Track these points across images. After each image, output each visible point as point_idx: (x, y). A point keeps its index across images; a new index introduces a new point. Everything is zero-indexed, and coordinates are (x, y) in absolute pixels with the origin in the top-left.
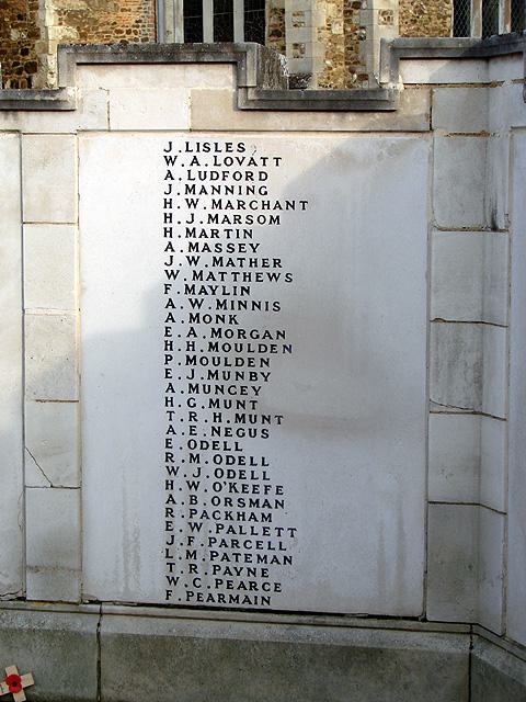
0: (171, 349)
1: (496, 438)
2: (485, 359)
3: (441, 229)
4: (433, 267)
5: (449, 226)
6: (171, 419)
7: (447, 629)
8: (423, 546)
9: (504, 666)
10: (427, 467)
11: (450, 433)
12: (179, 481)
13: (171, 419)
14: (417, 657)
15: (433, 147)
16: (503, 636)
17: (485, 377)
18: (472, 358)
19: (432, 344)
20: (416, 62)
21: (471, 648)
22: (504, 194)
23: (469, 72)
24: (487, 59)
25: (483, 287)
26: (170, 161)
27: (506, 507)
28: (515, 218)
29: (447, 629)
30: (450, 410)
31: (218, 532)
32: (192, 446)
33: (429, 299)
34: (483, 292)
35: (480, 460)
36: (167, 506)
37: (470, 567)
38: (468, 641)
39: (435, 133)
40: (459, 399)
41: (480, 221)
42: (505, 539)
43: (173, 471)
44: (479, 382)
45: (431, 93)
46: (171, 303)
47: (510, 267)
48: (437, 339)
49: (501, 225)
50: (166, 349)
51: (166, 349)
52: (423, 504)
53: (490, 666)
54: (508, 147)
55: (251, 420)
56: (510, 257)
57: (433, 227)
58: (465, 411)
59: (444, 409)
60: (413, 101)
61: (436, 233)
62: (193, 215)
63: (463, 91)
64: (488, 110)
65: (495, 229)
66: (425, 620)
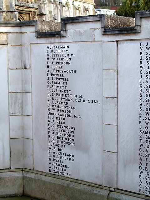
0: (146, 48)
1: (29, 121)
2: (24, 101)
3: (11, 69)
4: (9, 79)
5: (13, 68)
7: (16, 170)
8: (9, 150)
9: (35, 177)
10: (10, 130)
11: (15, 121)
14: (9, 178)
15: (8, 48)
16: (33, 170)
17: (24, 106)
18: (20, 101)
19: (10, 98)
20: (3, 27)
21: (23, 174)
22: (29, 60)
23: (17, 30)
24: (21, 27)
25: (22, 83)
27: (33, 137)
28: (32, 66)
29: (16, 170)
30: (15, 115)
32: (147, 129)
33: (8, 87)
34: (22, 85)
35: (23, 127)
37: (22, 154)
38: (22, 173)
39: (9, 45)
40: (17, 112)
41: (21, 67)
42: (33, 146)
43: (141, 145)
44: (22, 107)
45: (7, 35)
47: (31, 78)
48: (11, 97)
49: (28, 67)
52: (9, 139)
53: (30, 177)
54: (29, 48)
56: (31, 75)
57: (9, 69)
58: (19, 115)
59: (13, 115)
60: (3, 37)
61: (10, 70)
63: (15, 34)
64: (22, 39)
65: (26, 68)
66: (10, 169)
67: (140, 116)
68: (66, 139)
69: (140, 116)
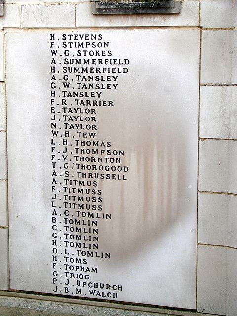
6: (54, 167)
12: (58, 156)
13: (54, 167)
26: (54, 53)
31: (84, 286)
36: (52, 65)
43: (54, 53)
46: (55, 173)
50: (52, 96)
51: (52, 96)
55: (87, 200)
62: (66, 148)
67: (53, 146)
68: (77, 95)
69: (53, 146)
